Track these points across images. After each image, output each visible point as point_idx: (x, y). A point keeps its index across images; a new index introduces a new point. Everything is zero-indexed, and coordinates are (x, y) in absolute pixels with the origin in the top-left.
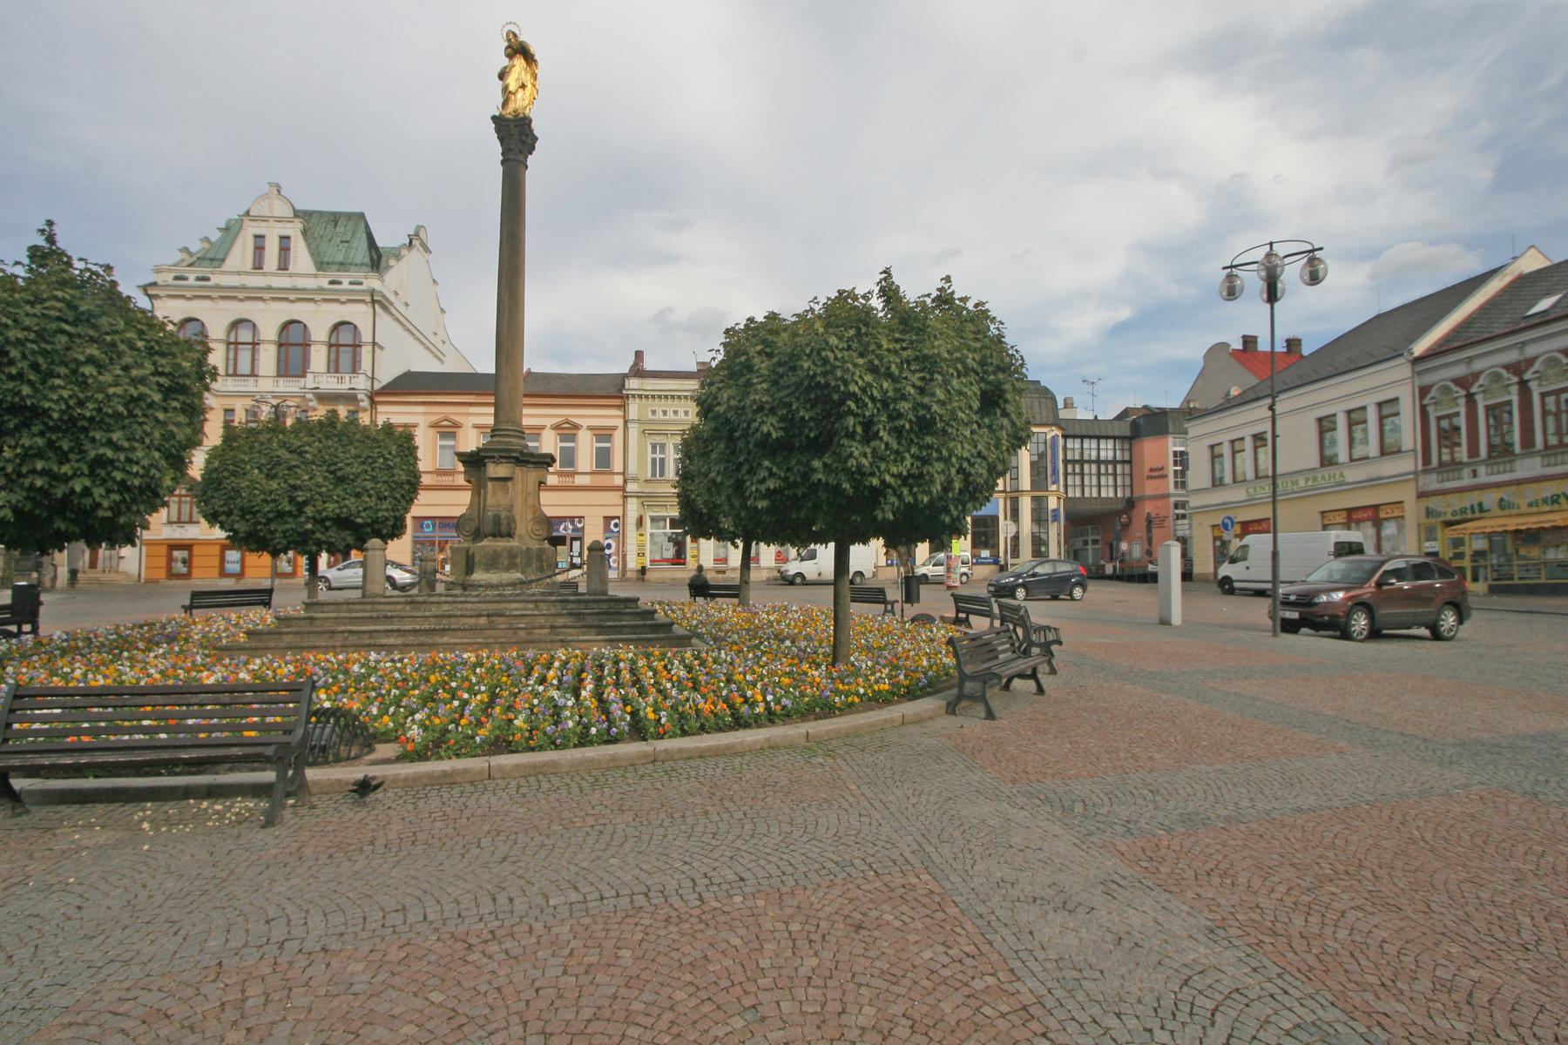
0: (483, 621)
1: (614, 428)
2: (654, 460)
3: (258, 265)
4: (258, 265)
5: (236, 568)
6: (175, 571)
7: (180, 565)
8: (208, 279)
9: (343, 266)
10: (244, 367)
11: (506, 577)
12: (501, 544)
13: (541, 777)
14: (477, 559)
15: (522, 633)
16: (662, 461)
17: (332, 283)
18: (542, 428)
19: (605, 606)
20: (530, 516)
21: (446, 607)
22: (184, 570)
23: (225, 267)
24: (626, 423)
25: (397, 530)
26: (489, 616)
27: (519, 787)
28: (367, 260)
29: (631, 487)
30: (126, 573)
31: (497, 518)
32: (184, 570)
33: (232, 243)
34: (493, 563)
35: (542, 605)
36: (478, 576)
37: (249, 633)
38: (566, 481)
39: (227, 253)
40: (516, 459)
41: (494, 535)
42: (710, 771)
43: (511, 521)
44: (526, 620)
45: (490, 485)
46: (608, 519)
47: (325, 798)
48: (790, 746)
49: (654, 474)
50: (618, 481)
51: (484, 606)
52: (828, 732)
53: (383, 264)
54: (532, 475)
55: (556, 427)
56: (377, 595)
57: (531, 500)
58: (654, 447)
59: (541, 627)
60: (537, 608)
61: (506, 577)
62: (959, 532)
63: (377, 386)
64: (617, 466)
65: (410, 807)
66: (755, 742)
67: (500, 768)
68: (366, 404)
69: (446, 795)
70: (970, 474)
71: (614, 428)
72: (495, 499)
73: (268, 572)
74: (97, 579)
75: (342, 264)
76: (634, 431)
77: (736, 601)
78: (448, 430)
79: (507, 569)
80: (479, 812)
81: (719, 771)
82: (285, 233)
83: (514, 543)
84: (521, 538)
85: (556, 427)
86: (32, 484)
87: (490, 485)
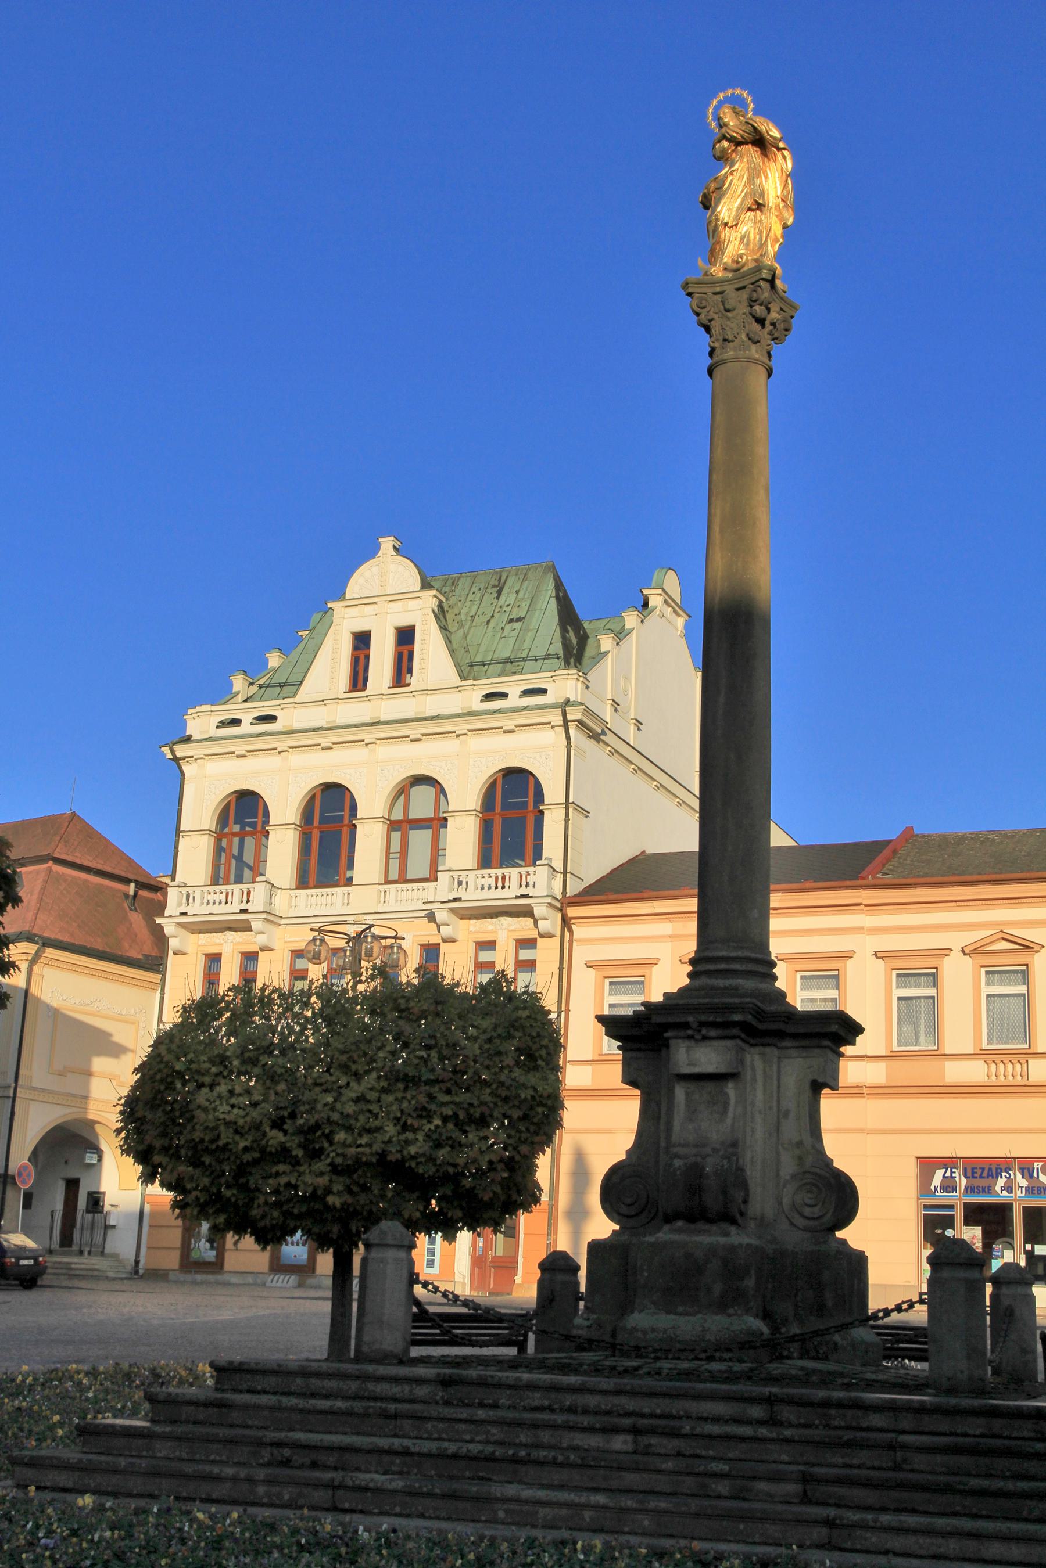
0: (620, 1443)
3: (358, 680)
4: (358, 680)
6: (195, 1255)
8: (272, 718)
9: (510, 664)
10: (418, 866)
11: (716, 1325)
12: (709, 1238)
15: (722, 1487)
18: (945, 952)
19: (976, 1426)
20: (788, 1167)
21: (537, 1398)
22: (211, 1255)
23: (305, 692)
26: (635, 1431)
28: (558, 648)
30: (115, 1256)
31: (695, 1171)
32: (211, 1255)
34: (683, 1285)
35: (787, 1413)
40: (744, 1026)
41: (691, 1219)
45: (680, 1092)
53: (589, 651)
54: (795, 1068)
55: (971, 951)
57: (791, 1130)
59: (776, 1478)
60: (773, 1422)
61: (716, 1325)
68: (551, 923)
72: (694, 1125)
74: (68, 1266)
75: (509, 661)
79: (722, 1306)
82: (405, 622)
83: (737, 1237)
84: (762, 1222)
85: (971, 951)
87: (680, 1092)
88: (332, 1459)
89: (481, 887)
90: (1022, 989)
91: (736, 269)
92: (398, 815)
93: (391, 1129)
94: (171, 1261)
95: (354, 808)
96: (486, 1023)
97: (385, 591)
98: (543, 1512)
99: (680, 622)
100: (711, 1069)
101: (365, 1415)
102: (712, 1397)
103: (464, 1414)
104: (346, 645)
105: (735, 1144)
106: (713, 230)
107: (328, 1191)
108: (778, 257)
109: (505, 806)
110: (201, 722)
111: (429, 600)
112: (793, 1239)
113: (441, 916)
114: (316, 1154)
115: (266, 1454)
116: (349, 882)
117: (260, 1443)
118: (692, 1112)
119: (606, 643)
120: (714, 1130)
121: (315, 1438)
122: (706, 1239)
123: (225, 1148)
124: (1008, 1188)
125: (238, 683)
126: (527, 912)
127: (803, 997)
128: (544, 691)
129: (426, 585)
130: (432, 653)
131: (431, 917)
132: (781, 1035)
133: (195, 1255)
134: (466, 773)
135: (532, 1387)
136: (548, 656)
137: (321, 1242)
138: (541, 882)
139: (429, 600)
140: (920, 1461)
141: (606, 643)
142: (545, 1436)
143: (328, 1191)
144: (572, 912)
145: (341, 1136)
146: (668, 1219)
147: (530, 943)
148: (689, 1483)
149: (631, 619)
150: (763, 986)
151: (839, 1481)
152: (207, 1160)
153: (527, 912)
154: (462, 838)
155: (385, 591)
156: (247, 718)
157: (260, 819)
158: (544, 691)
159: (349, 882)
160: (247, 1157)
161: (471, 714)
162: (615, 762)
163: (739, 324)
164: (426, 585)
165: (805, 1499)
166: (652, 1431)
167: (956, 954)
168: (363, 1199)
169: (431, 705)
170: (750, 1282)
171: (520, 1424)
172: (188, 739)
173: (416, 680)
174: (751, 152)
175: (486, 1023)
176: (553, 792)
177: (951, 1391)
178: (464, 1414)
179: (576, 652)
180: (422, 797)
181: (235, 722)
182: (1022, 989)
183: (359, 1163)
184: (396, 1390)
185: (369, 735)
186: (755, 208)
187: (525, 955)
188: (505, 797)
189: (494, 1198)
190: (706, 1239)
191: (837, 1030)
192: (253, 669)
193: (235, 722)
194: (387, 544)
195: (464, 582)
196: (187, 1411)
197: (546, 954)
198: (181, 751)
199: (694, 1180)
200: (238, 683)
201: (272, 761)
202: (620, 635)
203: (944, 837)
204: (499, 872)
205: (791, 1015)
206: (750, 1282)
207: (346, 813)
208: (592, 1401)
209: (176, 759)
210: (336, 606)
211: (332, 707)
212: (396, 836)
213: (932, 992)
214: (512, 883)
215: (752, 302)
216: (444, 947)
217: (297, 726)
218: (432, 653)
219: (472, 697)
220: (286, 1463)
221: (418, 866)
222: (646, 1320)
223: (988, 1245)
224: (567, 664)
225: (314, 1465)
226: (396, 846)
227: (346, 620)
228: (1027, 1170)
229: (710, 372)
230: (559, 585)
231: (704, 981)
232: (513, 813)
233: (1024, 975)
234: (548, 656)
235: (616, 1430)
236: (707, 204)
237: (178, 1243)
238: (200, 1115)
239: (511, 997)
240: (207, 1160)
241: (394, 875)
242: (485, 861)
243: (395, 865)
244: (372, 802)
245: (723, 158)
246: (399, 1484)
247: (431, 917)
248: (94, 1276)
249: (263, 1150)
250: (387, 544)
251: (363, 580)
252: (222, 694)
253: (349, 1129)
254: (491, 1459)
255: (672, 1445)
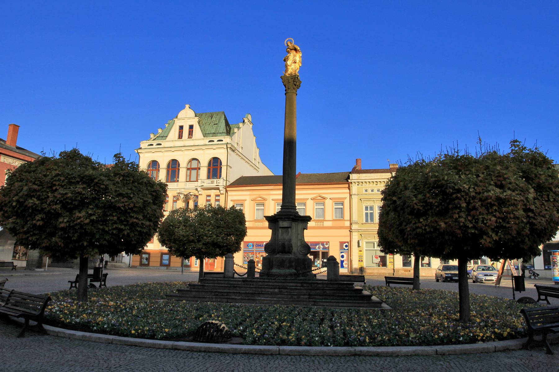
0: (277, 290)
1: (345, 198)
2: (367, 214)
3: (180, 136)
4: (180, 136)
5: (167, 262)
6: (143, 263)
7: (145, 260)
8: (161, 144)
9: (214, 134)
10: (193, 178)
11: (287, 271)
12: (286, 256)
13: (301, 356)
14: (274, 263)
15: (295, 297)
16: (372, 214)
17: (210, 141)
18: (307, 199)
19: (336, 286)
20: (299, 244)
21: (260, 283)
22: (147, 263)
23: (168, 139)
24: (351, 195)
25: (238, 249)
26: (279, 288)
27: (292, 359)
28: (225, 131)
29: (354, 227)
30: (125, 263)
32: (147, 263)
33: (170, 130)
34: (281, 264)
35: (305, 285)
36: (275, 271)
37: (178, 290)
38: (320, 224)
39: (168, 134)
40: (292, 218)
42: (382, 362)
43: (290, 246)
44: (297, 291)
45: (280, 230)
46: (342, 243)
47: (214, 354)
48: (428, 356)
49: (367, 220)
50: (347, 224)
51: (277, 284)
52: (448, 351)
53: (232, 132)
54: (300, 226)
56: (230, 277)
57: (299, 237)
58: (367, 208)
59: (304, 295)
60: (302, 286)
61: (287, 271)
62: (536, 253)
63: (228, 184)
64: (347, 217)
65: (247, 361)
66: (408, 352)
67: (283, 350)
68: (223, 191)
69: (261, 359)
70: (534, 224)
71: (345, 198)
72: (282, 236)
73: (180, 265)
74: (114, 265)
75: (214, 133)
76: (355, 199)
77: (411, 287)
78: (261, 203)
79: (288, 268)
80: (274, 366)
81: (386, 362)
82: (191, 124)
83: (291, 256)
84: (295, 253)
86: (112, 232)
87: (280, 230)
88: (225, 294)
89: (208, 183)
90: (323, 207)
91: (291, 74)
92: (189, 167)
93: (215, 236)
94: (138, 264)
95: (179, 165)
96: (233, 216)
97: (187, 116)
98: (265, 302)
99: (251, 126)
100: (286, 226)
101: (230, 287)
102: (292, 283)
103: (249, 286)
104: (178, 128)
105: (290, 239)
106: (286, 66)
107: (202, 248)
108: (298, 72)
109: (213, 165)
110: (144, 144)
111: (197, 119)
112: (300, 256)
113: (199, 189)
114: (199, 241)
115: (213, 294)
116: (178, 181)
117: (212, 292)
118: (282, 234)
119: (236, 130)
120: (287, 237)
121: (223, 291)
122: (286, 256)
123: (181, 240)
124: (319, 248)
125: (152, 136)
126: (218, 189)
127: (301, 214)
128: (222, 141)
129: (196, 116)
130: (197, 130)
131: (197, 189)
132: (298, 220)
133: (143, 263)
134: (205, 158)
135: (260, 282)
136: (223, 133)
137: (197, 258)
138: (221, 183)
139: (197, 119)
140: (328, 292)
141: (236, 130)
142: (263, 290)
143: (202, 248)
144: (228, 189)
145: (205, 238)
146: (278, 253)
147: (218, 196)
148: (289, 296)
149: (241, 125)
150: (292, 211)
151: (315, 295)
152: (177, 242)
153: (218, 189)
154: (204, 172)
155: (187, 116)
156: (155, 144)
157: (157, 167)
158: (222, 141)
159: (178, 181)
160: (186, 242)
161: (206, 145)
162: (237, 156)
163: (291, 85)
164: (196, 116)
165: (309, 298)
166: (282, 288)
167: (310, 199)
168: (208, 250)
169: (197, 143)
170: (294, 264)
171: (259, 288)
172: (141, 148)
173: (194, 136)
174: (294, 52)
175: (233, 216)
176: (224, 163)
177: (331, 281)
178: (249, 286)
179: (229, 132)
180: (195, 162)
181: (152, 145)
182: (323, 207)
183: (208, 243)
184: (235, 283)
185: (183, 149)
186: (294, 63)
187: (217, 198)
188: (213, 163)
189: (227, 250)
190: (286, 256)
191: (308, 219)
192: (155, 133)
193: (152, 145)
194: (187, 106)
195: (204, 115)
196: (197, 287)
197: (222, 198)
198: (139, 151)
199: (283, 246)
200: (152, 136)
201: (160, 154)
202: (239, 128)
203: (307, 174)
204: (212, 180)
205: (300, 216)
206: (294, 264)
207: (177, 166)
208: (270, 284)
209: (138, 153)
210: (176, 120)
211: (174, 142)
212: (189, 171)
213: (304, 207)
214: (215, 182)
215: (294, 81)
216: (199, 196)
217: (166, 146)
218: (197, 130)
219: (206, 141)
220: (217, 295)
221: (193, 178)
222: (275, 271)
223: (314, 260)
224: (227, 135)
225: (222, 295)
226: (188, 174)
227: (178, 123)
228: (323, 244)
229: (285, 94)
230: (225, 117)
231: (284, 210)
232: (215, 168)
233: (324, 205)
234: (223, 133)
235: (276, 288)
236: (285, 61)
237: (139, 260)
238: (176, 233)
239: (236, 210)
240: (177, 242)
241: (188, 180)
242: (209, 178)
243: (188, 178)
244: (183, 164)
245: (288, 52)
246: (239, 298)
247: (197, 189)
248: (120, 267)
249: (189, 240)
250: (187, 106)
251: (181, 114)
252: (148, 138)
253: (207, 236)
254: (255, 293)
255: (286, 290)
